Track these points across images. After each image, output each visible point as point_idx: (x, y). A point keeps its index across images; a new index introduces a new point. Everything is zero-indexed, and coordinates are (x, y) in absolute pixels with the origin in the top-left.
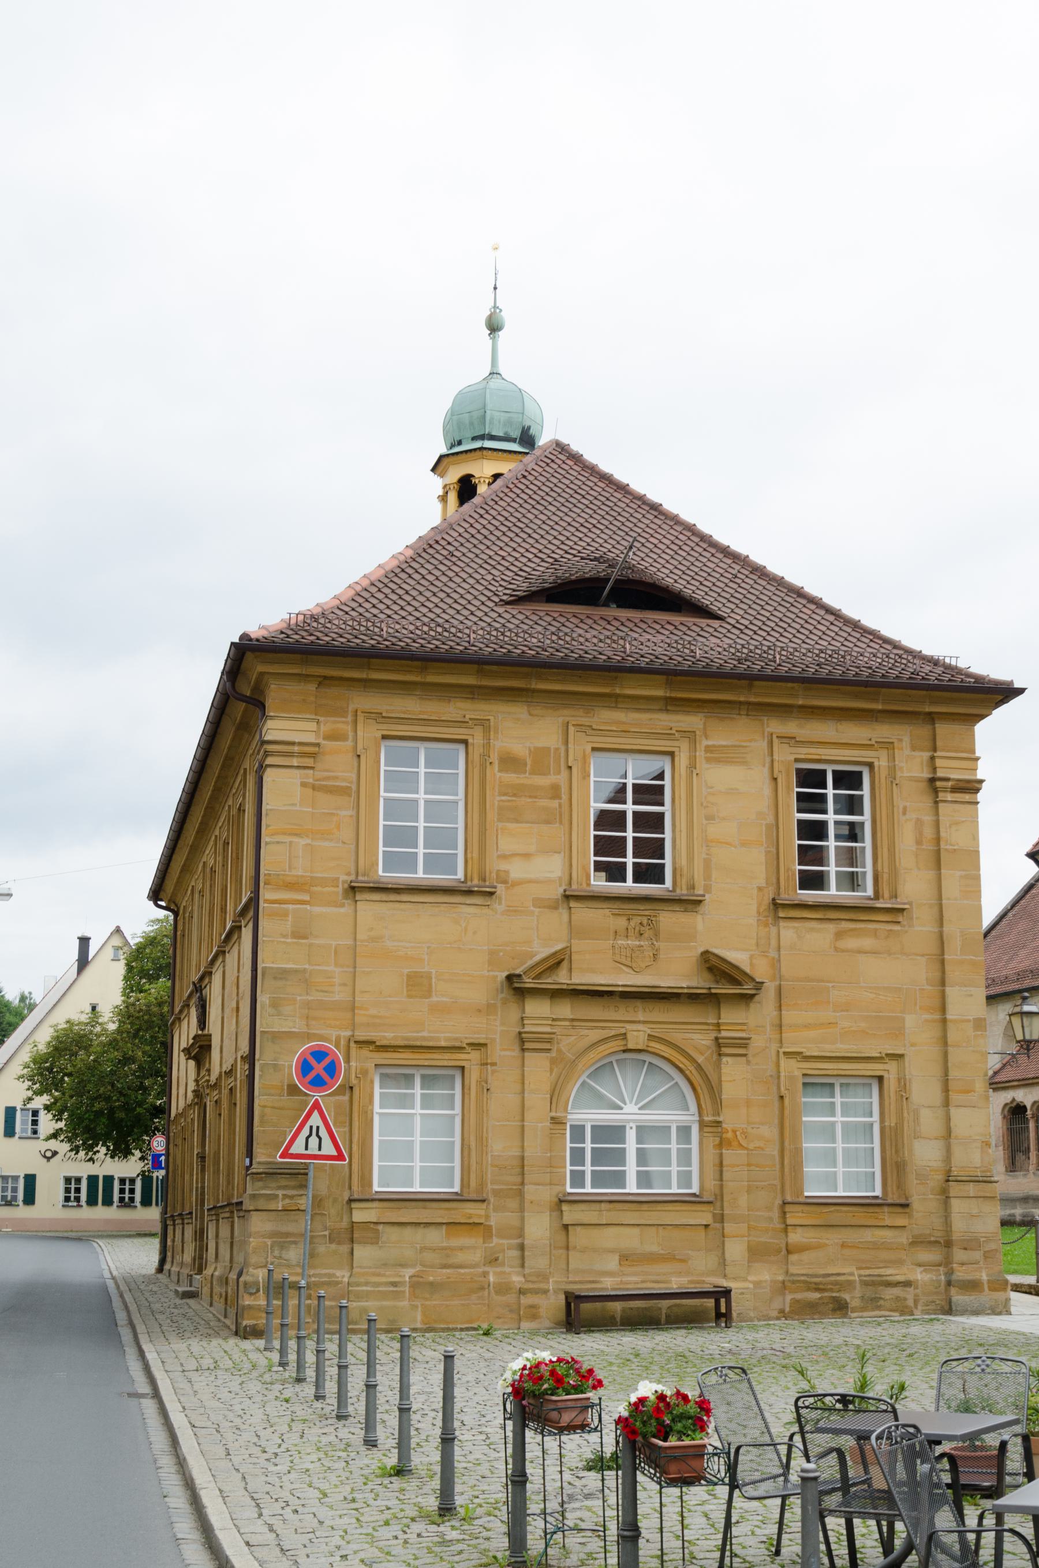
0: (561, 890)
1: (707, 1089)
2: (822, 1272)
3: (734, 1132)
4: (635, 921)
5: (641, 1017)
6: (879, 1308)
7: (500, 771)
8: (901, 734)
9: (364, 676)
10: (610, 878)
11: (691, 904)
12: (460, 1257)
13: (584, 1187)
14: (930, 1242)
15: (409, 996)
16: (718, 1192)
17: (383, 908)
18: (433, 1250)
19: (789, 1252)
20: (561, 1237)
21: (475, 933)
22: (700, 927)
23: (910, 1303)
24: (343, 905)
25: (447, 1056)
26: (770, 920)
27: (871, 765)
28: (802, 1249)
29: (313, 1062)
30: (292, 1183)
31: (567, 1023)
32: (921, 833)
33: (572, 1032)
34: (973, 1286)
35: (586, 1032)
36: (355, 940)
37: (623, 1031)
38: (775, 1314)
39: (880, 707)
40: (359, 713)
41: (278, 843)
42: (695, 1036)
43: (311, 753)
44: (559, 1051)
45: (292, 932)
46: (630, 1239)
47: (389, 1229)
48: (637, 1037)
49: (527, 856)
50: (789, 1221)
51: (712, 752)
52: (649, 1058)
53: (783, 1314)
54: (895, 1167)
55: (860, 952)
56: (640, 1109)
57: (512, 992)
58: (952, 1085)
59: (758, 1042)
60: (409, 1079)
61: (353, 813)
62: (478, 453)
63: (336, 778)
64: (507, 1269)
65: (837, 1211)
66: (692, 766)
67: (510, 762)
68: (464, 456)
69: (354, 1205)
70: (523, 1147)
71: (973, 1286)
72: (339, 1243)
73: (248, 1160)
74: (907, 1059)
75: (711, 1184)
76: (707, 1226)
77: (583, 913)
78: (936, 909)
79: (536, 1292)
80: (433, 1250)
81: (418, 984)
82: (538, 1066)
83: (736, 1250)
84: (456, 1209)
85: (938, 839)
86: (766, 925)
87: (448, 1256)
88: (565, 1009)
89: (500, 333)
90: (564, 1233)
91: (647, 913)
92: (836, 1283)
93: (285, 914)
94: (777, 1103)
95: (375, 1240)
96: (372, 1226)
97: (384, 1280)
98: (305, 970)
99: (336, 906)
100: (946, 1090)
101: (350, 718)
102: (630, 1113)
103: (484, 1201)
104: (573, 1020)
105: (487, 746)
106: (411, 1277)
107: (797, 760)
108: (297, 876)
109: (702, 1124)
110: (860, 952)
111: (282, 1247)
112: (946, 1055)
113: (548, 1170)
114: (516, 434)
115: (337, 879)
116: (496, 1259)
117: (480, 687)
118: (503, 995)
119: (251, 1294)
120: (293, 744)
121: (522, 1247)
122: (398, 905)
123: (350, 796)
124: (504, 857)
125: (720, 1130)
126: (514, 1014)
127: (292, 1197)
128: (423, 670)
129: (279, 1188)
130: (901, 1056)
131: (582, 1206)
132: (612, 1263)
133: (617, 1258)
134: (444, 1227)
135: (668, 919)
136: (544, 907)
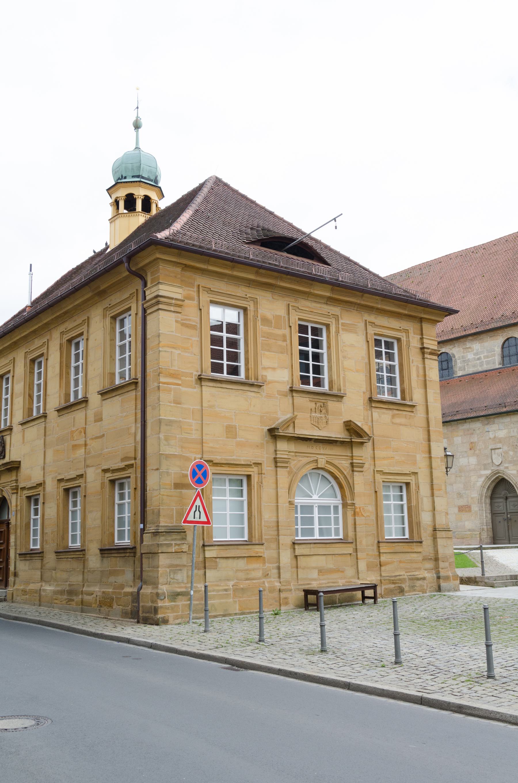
1: (344, 487)
2: (394, 575)
3: (360, 508)
4: (318, 404)
5: (322, 452)
6: (415, 590)
7: (261, 325)
8: (411, 326)
9: (206, 267)
11: (339, 397)
12: (253, 574)
14: (429, 559)
15: (227, 437)
16: (354, 538)
17: (213, 390)
18: (242, 571)
19: (381, 565)
21: (254, 406)
24: (195, 388)
25: (244, 469)
27: (399, 340)
29: (197, 470)
30: (179, 537)
31: (293, 454)
33: (295, 458)
34: (447, 578)
35: (301, 459)
36: (202, 406)
37: (316, 458)
39: (406, 312)
40: (200, 287)
41: (165, 351)
42: (343, 462)
44: (291, 468)
45: (174, 400)
46: (320, 562)
47: (222, 561)
48: (322, 463)
49: (274, 369)
50: (381, 551)
51: (344, 326)
54: (414, 524)
56: (319, 497)
57: (270, 437)
58: (435, 487)
59: (366, 466)
61: (199, 339)
62: (138, 183)
63: (190, 320)
64: (273, 580)
65: (398, 546)
66: (337, 332)
67: (266, 321)
68: (130, 184)
69: (206, 548)
70: (278, 516)
71: (447, 578)
74: (419, 474)
75: (351, 534)
77: (299, 400)
78: (424, 407)
80: (242, 571)
81: (231, 431)
83: (362, 565)
84: (251, 549)
85: (425, 375)
86: (367, 410)
87: (248, 574)
88: (292, 447)
89: (139, 130)
90: (295, 560)
91: (323, 401)
92: (400, 580)
93: (170, 390)
95: (215, 568)
96: (214, 559)
97: (221, 588)
98: (180, 421)
99: (192, 388)
100: (432, 489)
101: (195, 289)
103: (263, 544)
104: (296, 452)
105: (256, 311)
106: (232, 586)
108: (175, 370)
109: (345, 505)
111: (175, 573)
112: (431, 473)
113: (289, 528)
114: (153, 178)
115: (192, 373)
116: (268, 575)
117: (253, 281)
118: (266, 439)
119: (161, 600)
120: (172, 299)
121: (279, 568)
122: (220, 389)
124: (265, 368)
125: (354, 507)
127: (179, 545)
128: (233, 268)
129: (172, 540)
130: (416, 473)
132: (315, 574)
133: (317, 571)
134: (246, 558)
135: (332, 404)
136: (282, 395)
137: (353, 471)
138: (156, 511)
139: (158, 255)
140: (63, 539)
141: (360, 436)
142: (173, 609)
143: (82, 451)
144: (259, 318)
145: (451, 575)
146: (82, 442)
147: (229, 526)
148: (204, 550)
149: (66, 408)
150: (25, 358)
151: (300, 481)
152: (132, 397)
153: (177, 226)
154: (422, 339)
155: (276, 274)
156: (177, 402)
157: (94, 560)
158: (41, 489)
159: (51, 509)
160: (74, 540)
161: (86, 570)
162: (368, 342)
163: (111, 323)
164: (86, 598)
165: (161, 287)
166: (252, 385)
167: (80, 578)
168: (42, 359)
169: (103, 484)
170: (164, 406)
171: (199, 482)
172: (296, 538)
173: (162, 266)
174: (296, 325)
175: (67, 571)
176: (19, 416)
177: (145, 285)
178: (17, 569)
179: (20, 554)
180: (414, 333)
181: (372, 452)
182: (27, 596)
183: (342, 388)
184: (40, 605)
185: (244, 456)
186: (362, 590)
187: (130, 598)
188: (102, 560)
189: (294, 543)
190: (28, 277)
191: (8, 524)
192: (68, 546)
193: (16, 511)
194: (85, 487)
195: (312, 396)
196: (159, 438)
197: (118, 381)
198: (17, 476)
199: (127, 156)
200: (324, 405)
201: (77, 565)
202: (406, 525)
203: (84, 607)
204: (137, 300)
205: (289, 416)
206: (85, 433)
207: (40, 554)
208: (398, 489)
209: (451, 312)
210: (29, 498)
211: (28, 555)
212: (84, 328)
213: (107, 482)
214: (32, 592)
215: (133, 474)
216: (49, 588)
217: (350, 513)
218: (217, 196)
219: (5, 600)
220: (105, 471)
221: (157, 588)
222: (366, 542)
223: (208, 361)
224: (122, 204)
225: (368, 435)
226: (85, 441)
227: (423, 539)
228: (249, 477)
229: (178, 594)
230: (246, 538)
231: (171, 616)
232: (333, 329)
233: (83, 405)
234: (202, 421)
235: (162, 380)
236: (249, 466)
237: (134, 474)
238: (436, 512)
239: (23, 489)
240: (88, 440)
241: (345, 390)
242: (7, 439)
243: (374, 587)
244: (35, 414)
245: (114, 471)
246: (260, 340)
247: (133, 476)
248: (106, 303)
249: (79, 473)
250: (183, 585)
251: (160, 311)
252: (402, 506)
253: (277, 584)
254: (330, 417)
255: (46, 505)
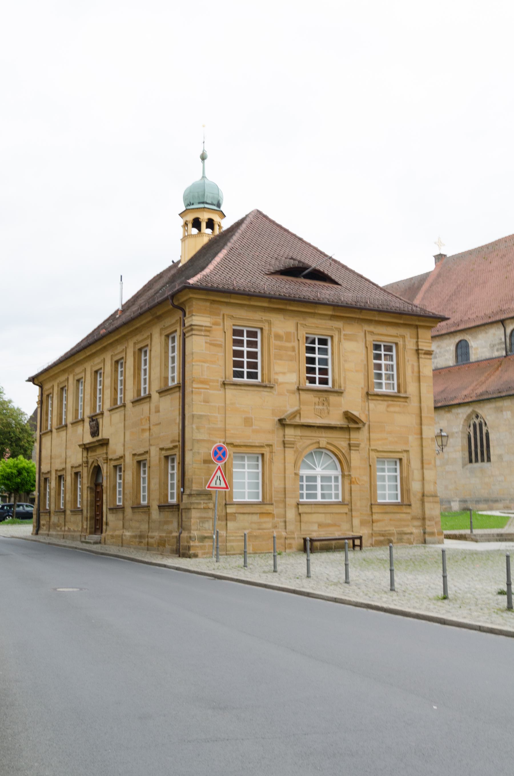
0: (296, 387)
1: (343, 462)
4: (321, 399)
6: (402, 542)
8: (408, 333)
10: (310, 383)
11: (340, 393)
12: (264, 526)
13: (332, 499)
16: (350, 500)
17: (235, 392)
19: (373, 522)
20: (298, 518)
22: (343, 402)
23: (412, 540)
24: (220, 390)
26: (366, 400)
27: (396, 344)
28: (378, 521)
29: (218, 451)
32: (413, 369)
34: (432, 534)
38: (369, 545)
39: (402, 322)
43: (208, 330)
44: (297, 448)
46: (321, 518)
47: (240, 516)
48: (323, 443)
49: (284, 373)
50: (373, 511)
52: (324, 451)
53: (372, 545)
54: (405, 491)
55: (395, 412)
59: (362, 445)
60: (243, 458)
63: (217, 340)
64: (280, 530)
66: (340, 341)
67: (278, 337)
69: (227, 506)
71: (432, 534)
72: (222, 521)
73: (182, 490)
75: (347, 498)
76: (346, 513)
77: (304, 396)
78: (418, 398)
79: (291, 538)
81: (248, 421)
82: (290, 454)
83: (356, 522)
86: (364, 402)
88: (298, 432)
92: (389, 534)
94: (368, 468)
95: (235, 520)
97: (238, 535)
101: (221, 317)
102: (319, 471)
104: (301, 436)
105: (270, 330)
107: (374, 341)
109: (343, 476)
110: (395, 412)
111: (203, 522)
114: (215, 202)
117: (268, 307)
119: (193, 541)
120: (202, 326)
121: (285, 522)
123: (222, 347)
124: (276, 373)
126: (281, 433)
127: (206, 503)
128: (250, 300)
129: (201, 500)
131: (306, 506)
132: (315, 527)
133: (317, 525)
135: (333, 399)
137: (350, 449)
138: (190, 479)
139: (191, 295)
140: (137, 497)
141: (355, 422)
142: (201, 548)
143: (147, 434)
144: (273, 335)
145: (436, 531)
146: (147, 427)
147: (247, 490)
148: (226, 508)
149: (138, 401)
150: (112, 359)
151: (305, 457)
152: (177, 395)
153: (207, 271)
154: (417, 342)
155: (286, 302)
156: (206, 401)
157: (155, 513)
158: (122, 460)
159: (129, 476)
160: (172, 498)
161: (150, 521)
162: (367, 348)
163: (165, 340)
164: (151, 540)
165: (194, 318)
166: (266, 387)
167: (147, 526)
168: (123, 361)
169: (160, 459)
170: (196, 406)
171: (220, 459)
172: (301, 500)
173: (194, 302)
174: (303, 337)
175: (139, 521)
176: (107, 405)
177: (185, 315)
178: (108, 520)
179: (109, 509)
180: (411, 338)
181: (368, 435)
182: (114, 540)
183: (343, 385)
184: (122, 546)
185: (257, 439)
186: (353, 539)
187: (175, 540)
188: (160, 514)
189: (298, 504)
190: (119, 286)
191: (102, 486)
192: (140, 504)
193: (107, 476)
194: (150, 460)
195: (316, 393)
196: (192, 428)
197: (170, 384)
198: (107, 450)
199: (194, 186)
200: (327, 400)
201: (145, 517)
202: (399, 492)
203: (149, 547)
204: (180, 325)
205: (296, 408)
206: (149, 421)
207: (122, 509)
208: (394, 463)
209: (443, 319)
210: (115, 467)
211: (115, 509)
212: (148, 342)
213: (162, 457)
214: (118, 536)
215: (177, 453)
216: (128, 534)
217: (347, 482)
218: (259, 223)
219: (100, 543)
220: (162, 449)
221: (190, 533)
222: (360, 504)
223: (231, 369)
224: (190, 225)
225: (363, 422)
226: (150, 427)
227: (413, 503)
228: (263, 455)
229: (205, 538)
230: (260, 500)
231: (200, 552)
232: (336, 339)
233: (148, 400)
234: (225, 414)
235: (195, 386)
236: (262, 447)
237: (177, 452)
238: (425, 482)
239: (111, 460)
240: (151, 425)
241: (345, 387)
242: (100, 421)
243: (360, 538)
244: (119, 403)
245: (167, 450)
246: (273, 351)
247: (178, 454)
248: (161, 325)
249: (146, 450)
250: (209, 531)
251: (193, 336)
252: (396, 476)
253: (284, 534)
254: (331, 408)
255: (126, 472)
